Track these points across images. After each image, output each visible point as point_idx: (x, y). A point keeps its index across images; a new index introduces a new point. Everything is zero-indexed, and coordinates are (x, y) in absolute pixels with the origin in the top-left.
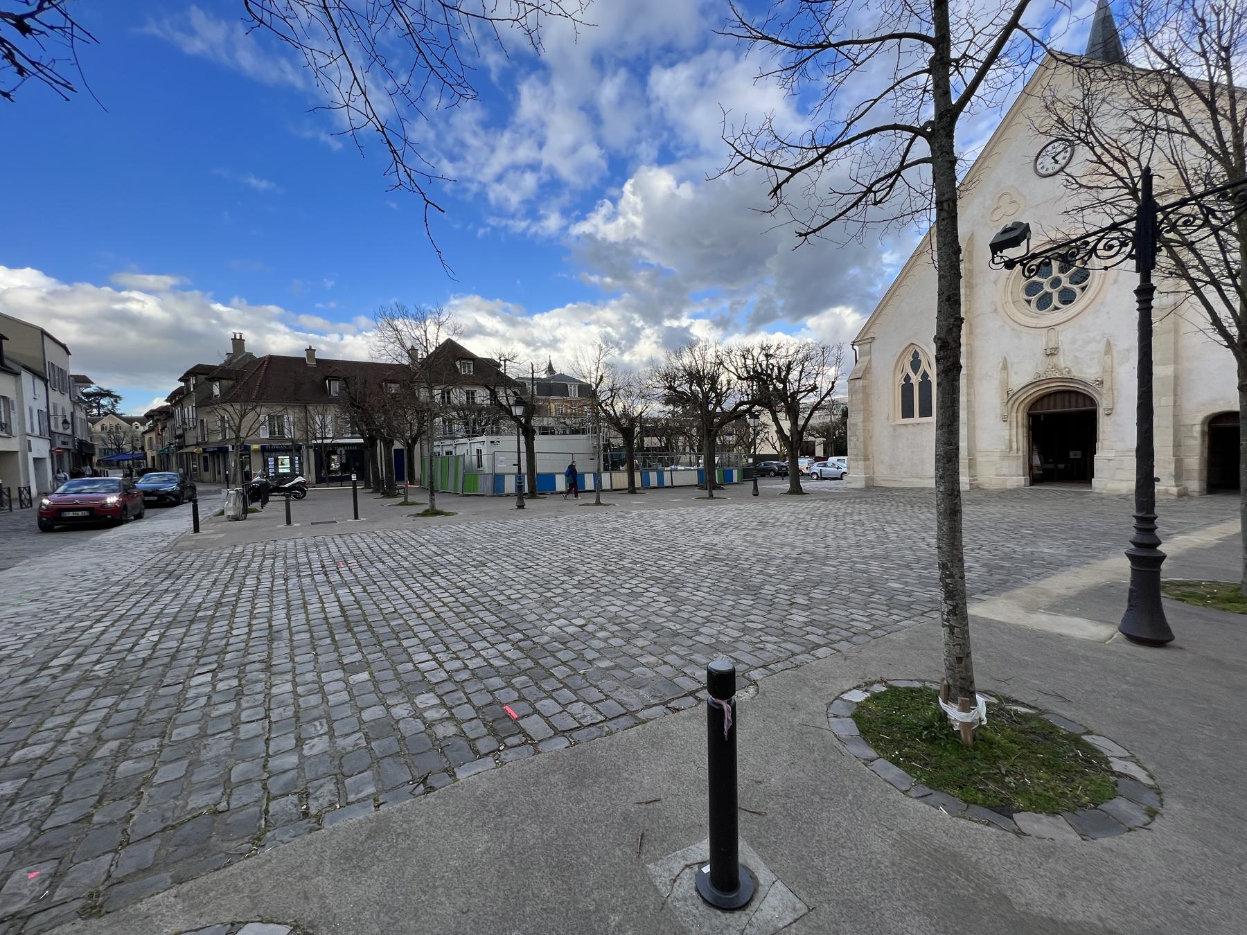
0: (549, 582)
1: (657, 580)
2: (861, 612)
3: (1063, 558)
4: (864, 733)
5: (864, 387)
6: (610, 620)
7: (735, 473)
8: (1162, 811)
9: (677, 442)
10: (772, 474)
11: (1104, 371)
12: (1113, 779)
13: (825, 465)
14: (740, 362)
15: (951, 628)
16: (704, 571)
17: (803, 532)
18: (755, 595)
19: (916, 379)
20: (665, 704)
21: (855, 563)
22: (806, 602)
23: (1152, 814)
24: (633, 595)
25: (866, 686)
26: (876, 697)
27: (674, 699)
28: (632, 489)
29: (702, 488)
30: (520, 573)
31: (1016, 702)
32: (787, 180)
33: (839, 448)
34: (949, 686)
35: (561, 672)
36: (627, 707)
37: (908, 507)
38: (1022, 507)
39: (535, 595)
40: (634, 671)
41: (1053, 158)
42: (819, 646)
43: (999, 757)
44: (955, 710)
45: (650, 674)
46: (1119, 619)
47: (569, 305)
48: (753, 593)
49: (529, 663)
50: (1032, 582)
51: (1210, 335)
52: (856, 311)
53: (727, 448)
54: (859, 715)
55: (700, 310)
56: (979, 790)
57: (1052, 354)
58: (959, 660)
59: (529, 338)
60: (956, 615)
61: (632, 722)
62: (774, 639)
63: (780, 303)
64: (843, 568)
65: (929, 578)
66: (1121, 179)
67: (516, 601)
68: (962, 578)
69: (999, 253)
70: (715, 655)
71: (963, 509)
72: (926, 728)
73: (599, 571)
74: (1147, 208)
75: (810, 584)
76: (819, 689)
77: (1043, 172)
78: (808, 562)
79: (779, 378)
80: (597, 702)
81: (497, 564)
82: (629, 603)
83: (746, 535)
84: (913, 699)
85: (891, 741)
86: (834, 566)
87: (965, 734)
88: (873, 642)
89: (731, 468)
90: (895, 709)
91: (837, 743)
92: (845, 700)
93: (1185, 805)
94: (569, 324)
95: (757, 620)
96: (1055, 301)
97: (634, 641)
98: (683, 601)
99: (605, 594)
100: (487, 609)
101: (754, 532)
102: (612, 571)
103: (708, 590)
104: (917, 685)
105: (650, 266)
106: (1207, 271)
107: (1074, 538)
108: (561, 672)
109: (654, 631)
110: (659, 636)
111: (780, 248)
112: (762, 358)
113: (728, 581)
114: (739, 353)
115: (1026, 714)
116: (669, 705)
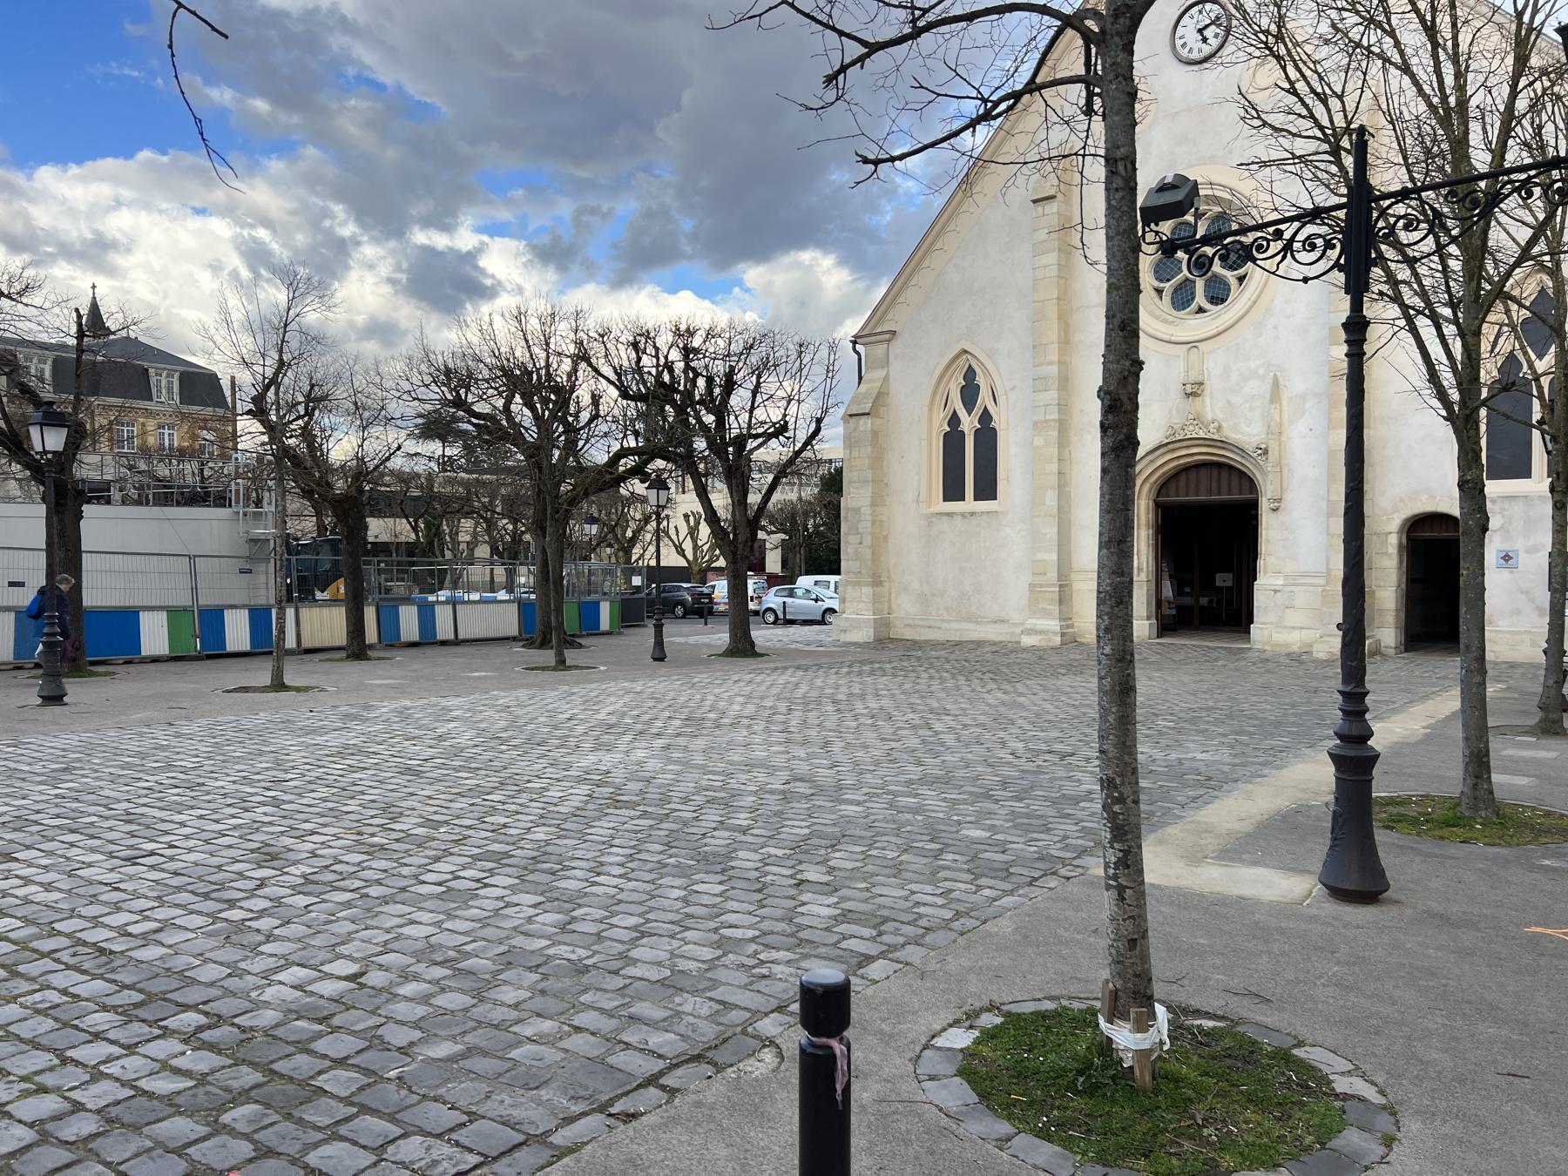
0: (222, 886)
1: (500, 857)
2: (928, 889)
3: (1226, 768)
4: (984, 1096)
5: (875, 434)
6: (419, 956)
7: (605, 609)
8: (1399, 1135)
9: (454, 535)
10: (679, 610)
11: (1269, 432)
12: (1338, 1104)
13: (791, 594)
14: (625, 357)
15: (1121, 889)
16: (601, 830)
17: (781, 737)
18: (723, 871)
19: (969, 424)
20: (602, 1109)
21: (895, 794)
22: (826, 878)
23: (1389, 1142)
24: (451, 896)
25: (969, 1018)
26: (990, 1035)
27: (618, 1097)
28: (357, 649)
29: (530, 643)
30: (131, 870)
31: (1197, 1013)
32: (861, 60)
33: (825, 560)
34: (1116, 991)
35: (339, 1082)
36: (525, 1128)
37: (962, 680)
38: (1150, 678)
39: (198, 921)
40: (514, 1054)
41: (1200, 31)
42: (869, 959)
43: (1190, 1100)
44: (1126, 1033)
45: (550, 1055)
46: (1318, 866)
47: (145, 155)
48: (718, 868)
49: (249, 1076)
50: (1187, 813)
51: (1427, 398)
52: (842, 262)
53: (586, 551)
54: (970, 1068)
55: (504, 215)
56: (1171, 1154)
57: (1194, 394)
58: (1132, 943)
59: (18, 228)
60: (1128, 867)
61: (546, 1154)
62: (783, 955)
63: (687, 224)
64: (877, 806)
65: (1027, 816)
66: (1322, 128)
67: (146, 939)
68: (1136, 802)
69: (1153, 226)
70: (677, 1000)
71: (1540, 690)
72: (1080, 1072)
73: (349, 850)
74: (1361, 194)
75: (823, 843)
76: (891, 1036)
77: (1184, 53)
78: (808, 797)
79: (708, 402)
80: (452, 1130)
81: (51, 853)
82: (450, 916)
83: (667, 747)
84: (1048, 1028)
85: (1031, 1104)
86: (859, 804)
87: (1142, 1072)
88: (961, 941)
89: (593, 597)
90: (1025, 1051)
91: (945, 1121)
92: (939, 1049)
93: (1424, 1122)
94: (147, 206)
95: (741, 921)
96: (1200, 299)
97: (492, 994)
98: (576, 900)
99: (385, 900)
100: (68, 967)
101: (682, 741)
102: (382, 848)
103: (622, 871)
104: (1049, 1006)
105: (379, 87)
106: (1423, 294)
107: (1237, 734)
108: (339, 1082)
109: (530, 969)
110: (545, 977)
111: (687, 98)
112: (675, 355)
113: (660, 848)
114: (627, 337)
115: (1214, 1028)
116: (613, 1110)
